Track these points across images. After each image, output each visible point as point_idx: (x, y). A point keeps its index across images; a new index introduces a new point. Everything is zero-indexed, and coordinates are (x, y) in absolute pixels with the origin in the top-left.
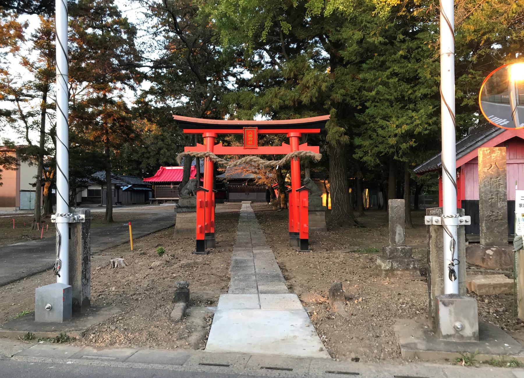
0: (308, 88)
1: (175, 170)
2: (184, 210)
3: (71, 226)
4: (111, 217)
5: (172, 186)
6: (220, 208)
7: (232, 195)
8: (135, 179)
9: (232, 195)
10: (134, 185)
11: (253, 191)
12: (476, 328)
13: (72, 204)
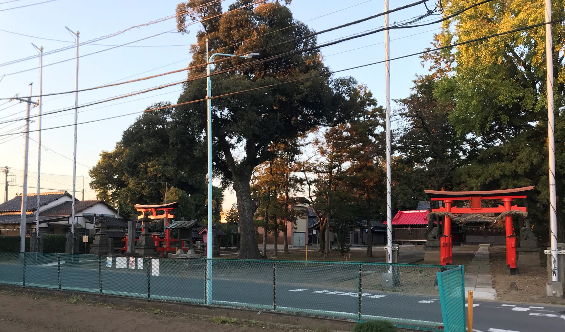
0: (522, 163)
1: (412, 213)
2: (430, 248)
3: (393, 251)
4: (371, 254)
5: (409, 229)
6: (456, 250)
7: (469, 238)
8: (375, 222)
9: (469, 238)
10: (375, 228)
11: (491, 234)
12: (562, 294)
13: (393, 242)
